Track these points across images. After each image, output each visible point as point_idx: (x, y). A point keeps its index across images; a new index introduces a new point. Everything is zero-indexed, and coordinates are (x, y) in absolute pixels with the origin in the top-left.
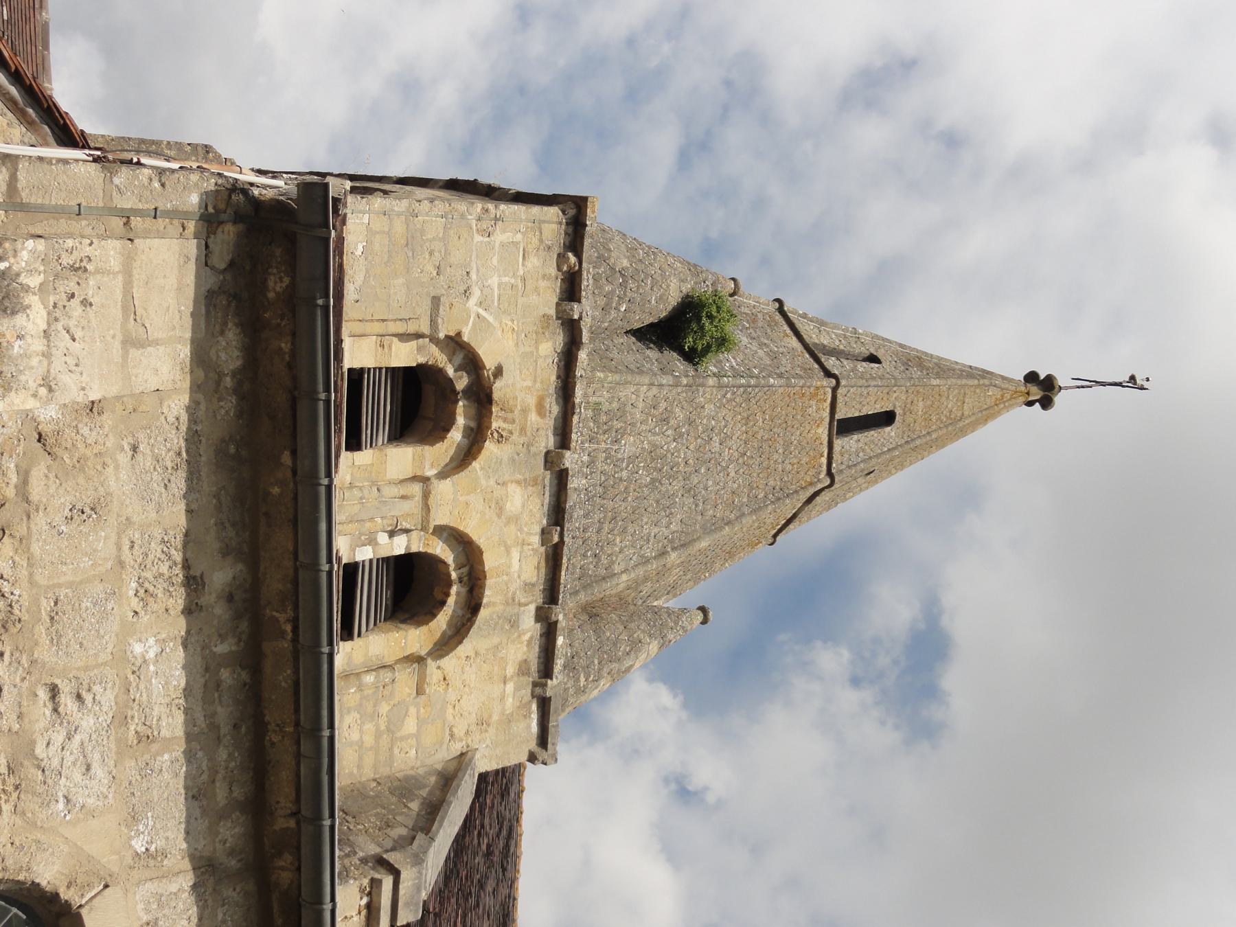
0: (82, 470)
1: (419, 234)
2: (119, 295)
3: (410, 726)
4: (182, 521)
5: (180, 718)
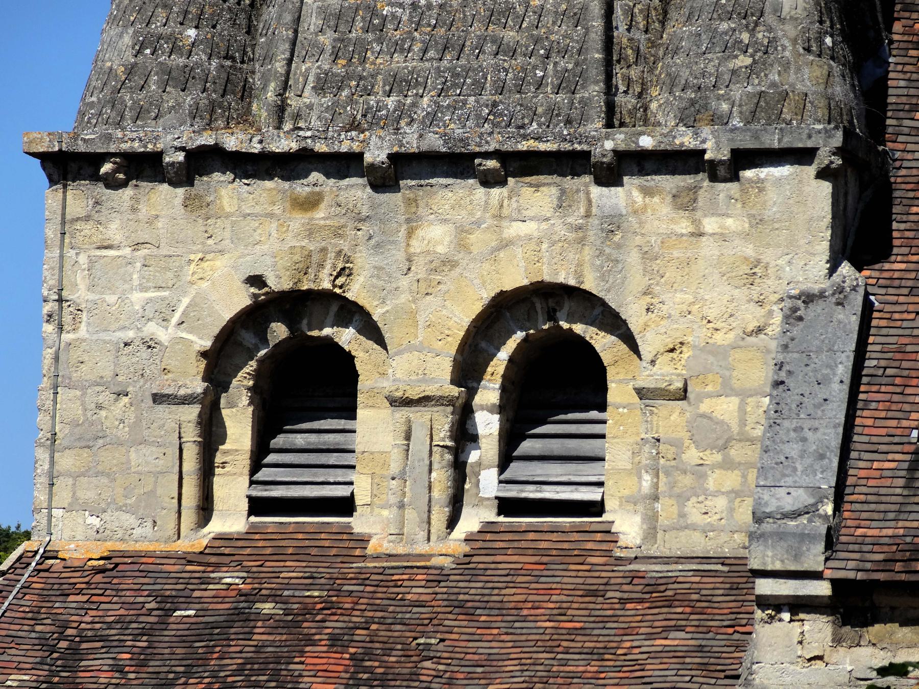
1: (77, 430)
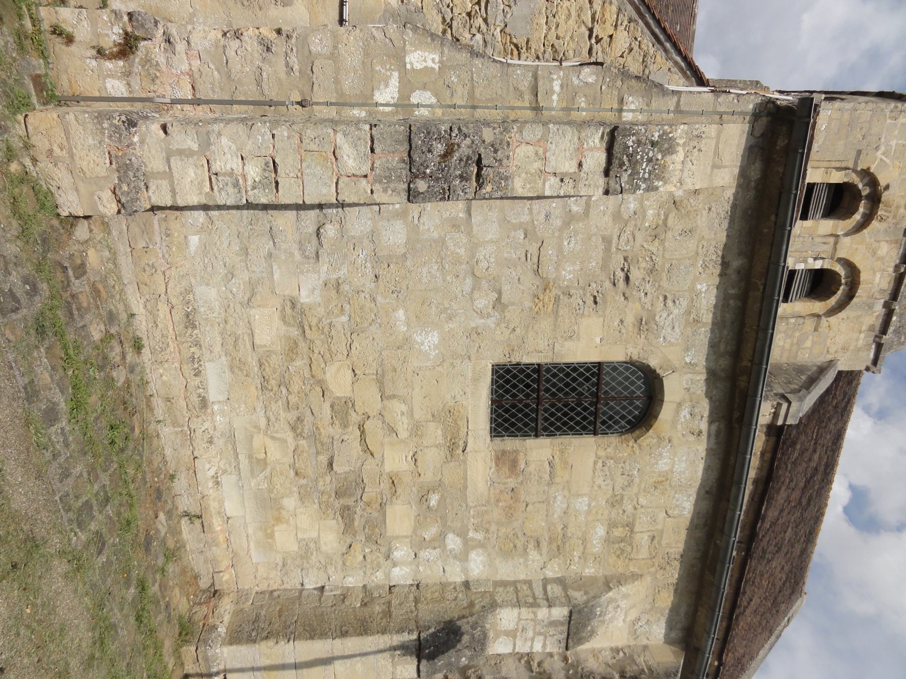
0: (688, 216)
2: (713, 146)
3: (808, 344)
4: (724, 239)
5: (711, 315)
